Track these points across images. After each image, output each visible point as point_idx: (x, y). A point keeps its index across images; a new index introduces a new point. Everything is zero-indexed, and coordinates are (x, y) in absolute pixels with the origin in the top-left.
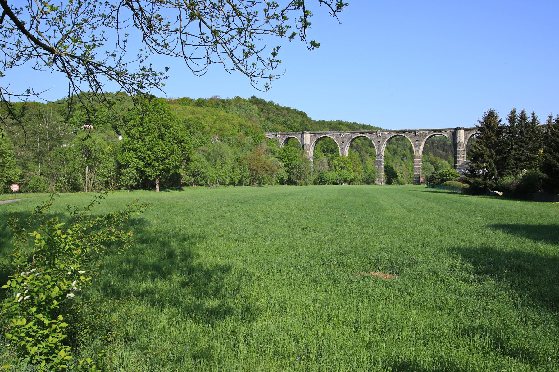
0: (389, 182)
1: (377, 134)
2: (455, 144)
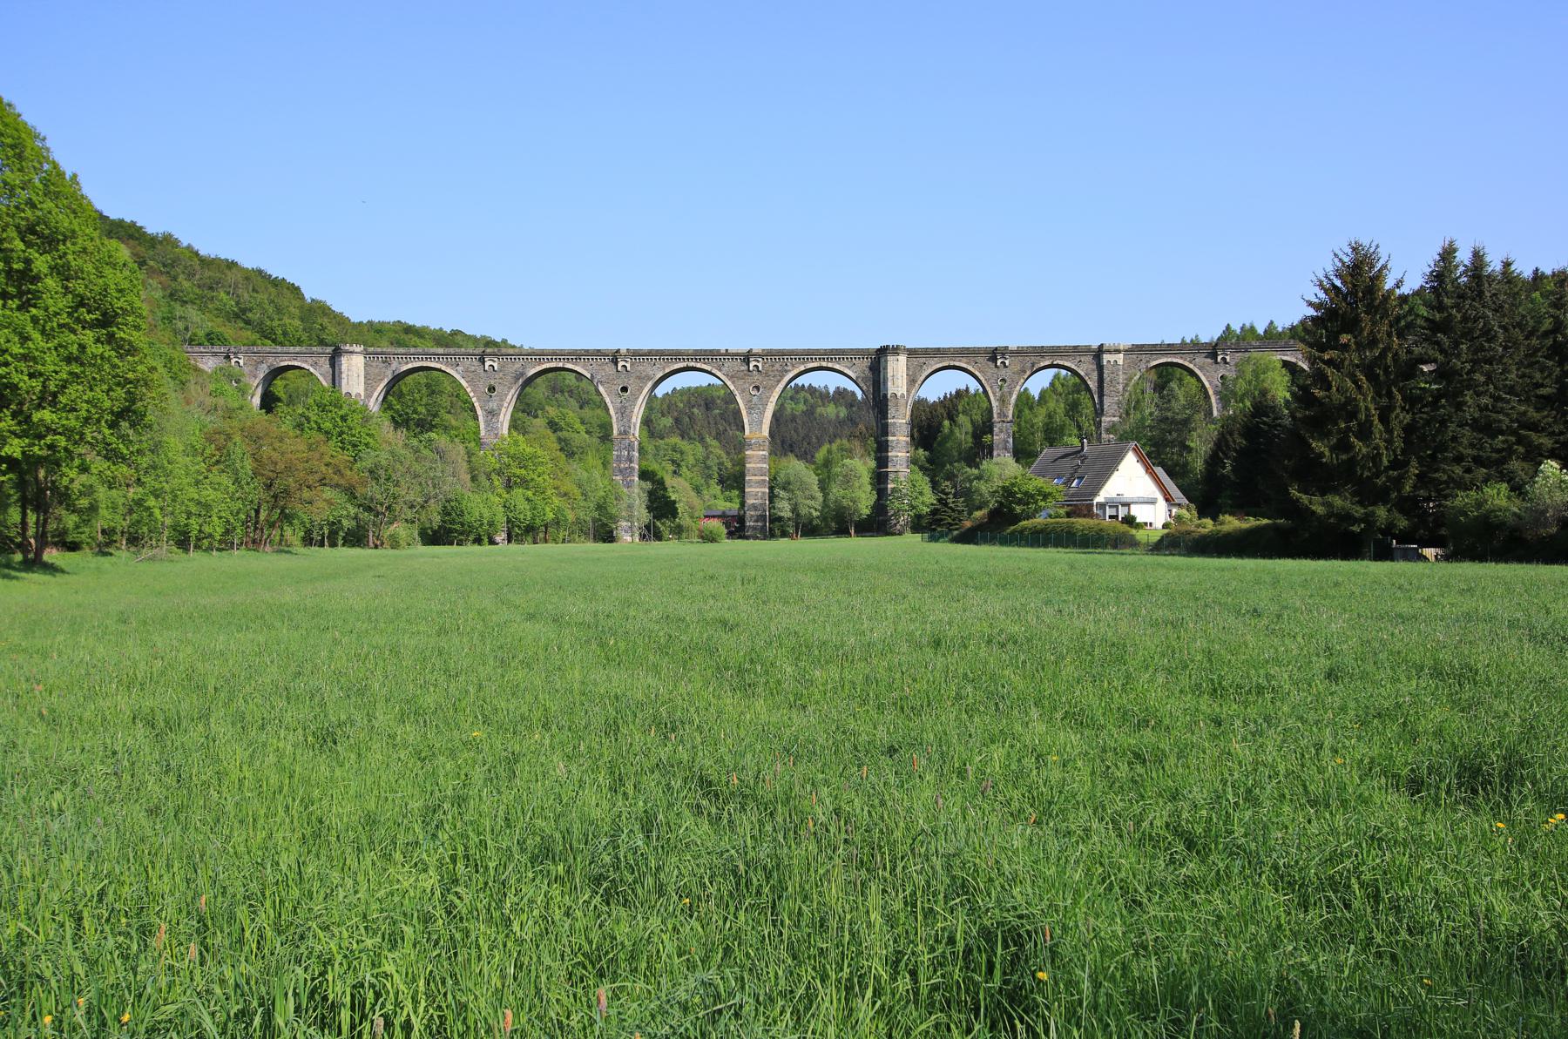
0: (651, 533)
1: (616, 364)
2: (879, 401)
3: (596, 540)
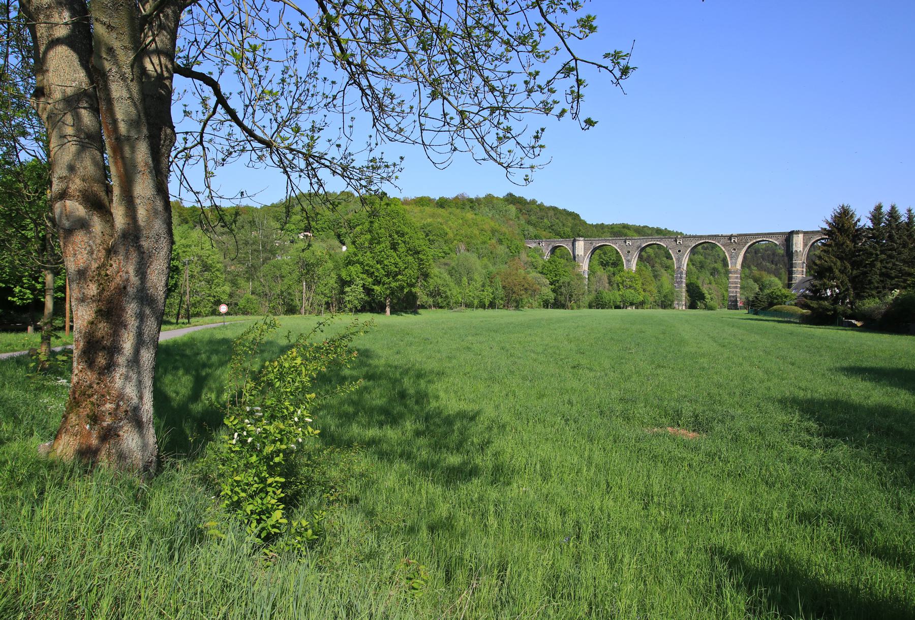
3: (662, 308)
